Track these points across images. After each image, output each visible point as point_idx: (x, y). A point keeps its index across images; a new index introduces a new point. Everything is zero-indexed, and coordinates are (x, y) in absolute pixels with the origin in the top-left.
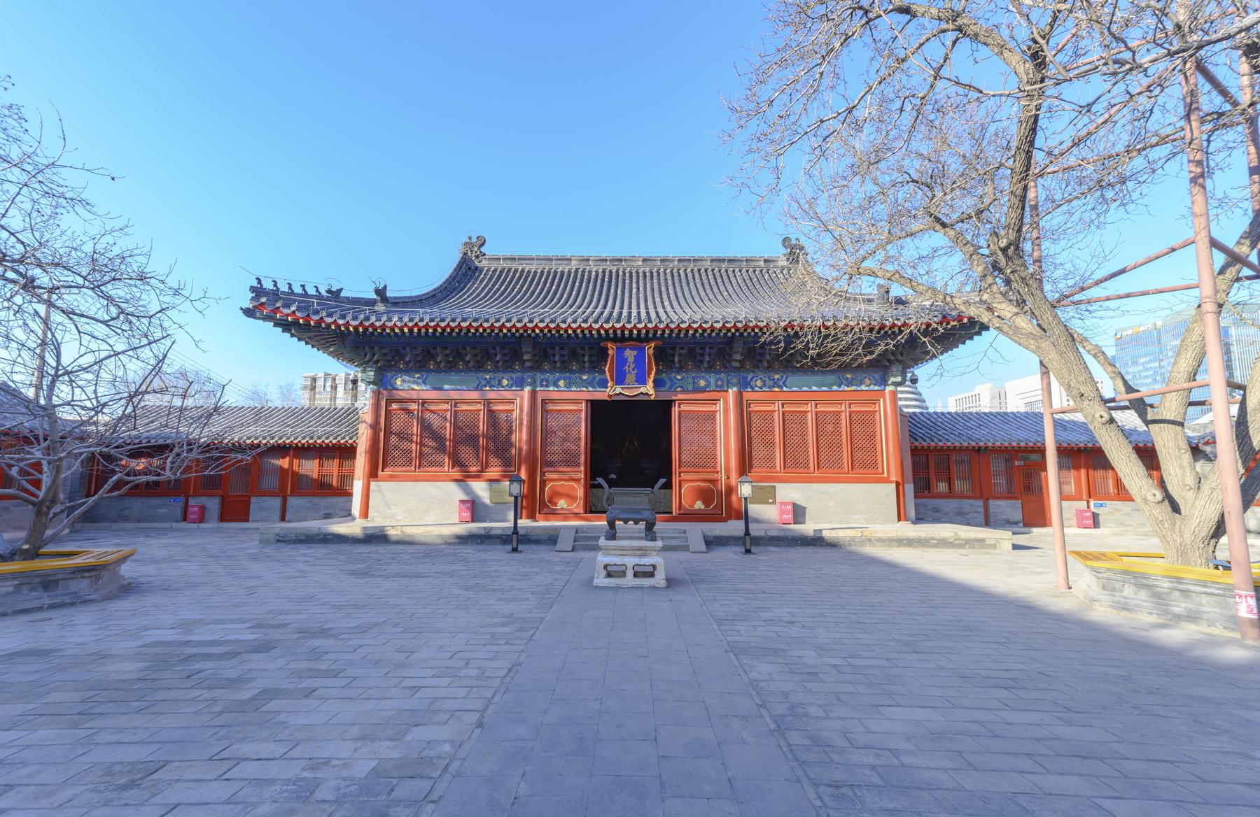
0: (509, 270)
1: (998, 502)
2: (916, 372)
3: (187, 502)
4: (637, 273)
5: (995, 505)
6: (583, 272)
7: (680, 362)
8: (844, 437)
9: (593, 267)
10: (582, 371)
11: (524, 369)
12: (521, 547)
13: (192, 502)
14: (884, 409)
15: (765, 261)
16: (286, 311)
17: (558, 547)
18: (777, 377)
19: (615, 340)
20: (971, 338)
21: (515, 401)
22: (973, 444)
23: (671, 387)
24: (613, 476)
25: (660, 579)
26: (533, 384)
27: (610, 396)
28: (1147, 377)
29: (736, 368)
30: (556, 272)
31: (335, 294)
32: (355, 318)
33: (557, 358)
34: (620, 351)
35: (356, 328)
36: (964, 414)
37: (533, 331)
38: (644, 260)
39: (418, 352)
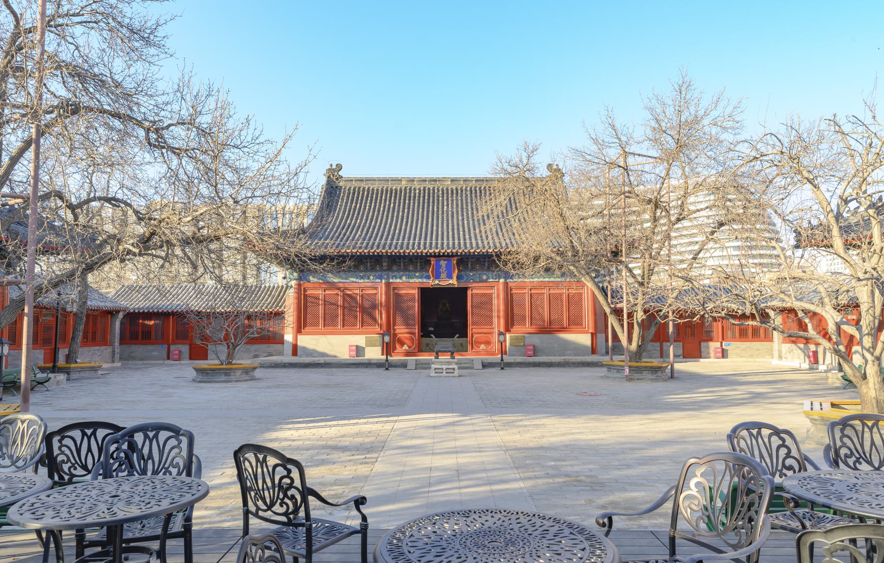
4: (447, 189)
9: (416, 185)
10: (415, 271)
11: (382, 270)
13: (172, 348)
19: (435, 256)
21: (372, 286)
30: (391, 190)
34: (438, 262)
38: (452, 181)
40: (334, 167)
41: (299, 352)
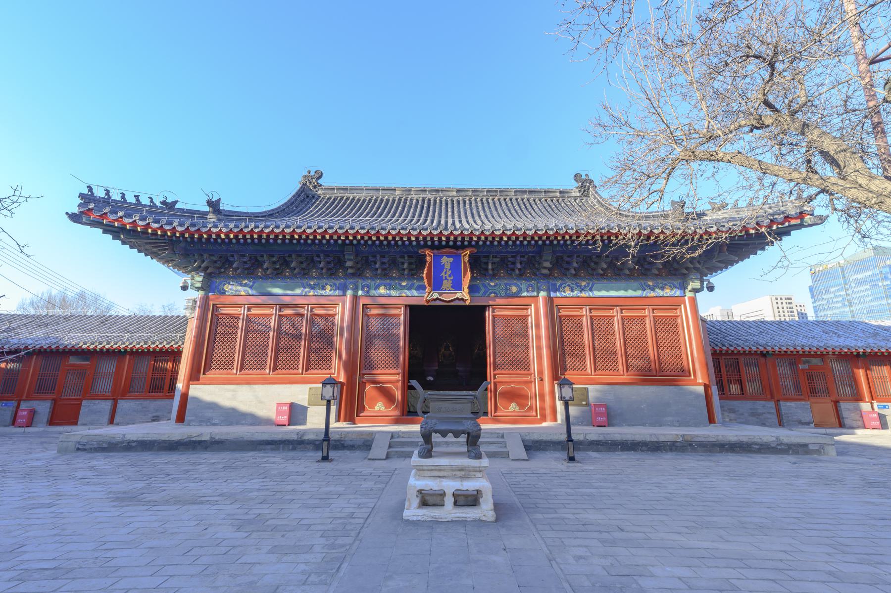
0: (342, 198)
1: (788, 404)
2: (712, 280)
3: (18, 406)
4: (452, 201)
5: (785, 406)
6: (406, 200)
7: (493, 269)
8: (650, 340)
10: (401, 277)
12: (332, 454)
14: (685, 312)
15: (561, 192)
16: (112, 217)
17: (373, 453)
18: (583, 284)
19: (433, 247)
20: (763, 249)
21: (337, 304)
22: (762, 348)
23: (485, 293)
24: (430, 378)
25: (486, 510)
26: (356, 289)
27: (428, 301)
28: (837, 302)
29: (545, 275)
30: (382, 200)
31: (170, 206)
32: (181, 225)
33: (378, 265)
34: (437, 258)
35: (182, 234)
36: (744, 322)
37: (355, 237)
38: (458, 191)
39: (246, 259)
40: (312, 173)
41: (188, 417)
